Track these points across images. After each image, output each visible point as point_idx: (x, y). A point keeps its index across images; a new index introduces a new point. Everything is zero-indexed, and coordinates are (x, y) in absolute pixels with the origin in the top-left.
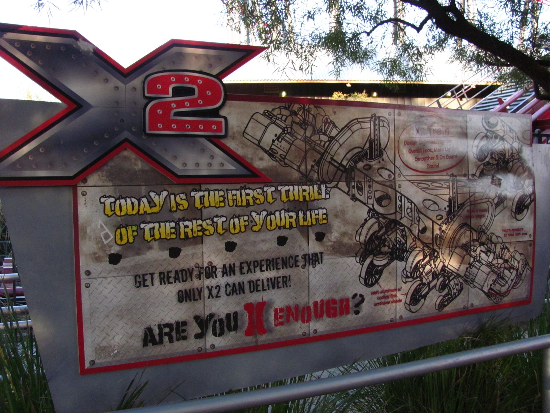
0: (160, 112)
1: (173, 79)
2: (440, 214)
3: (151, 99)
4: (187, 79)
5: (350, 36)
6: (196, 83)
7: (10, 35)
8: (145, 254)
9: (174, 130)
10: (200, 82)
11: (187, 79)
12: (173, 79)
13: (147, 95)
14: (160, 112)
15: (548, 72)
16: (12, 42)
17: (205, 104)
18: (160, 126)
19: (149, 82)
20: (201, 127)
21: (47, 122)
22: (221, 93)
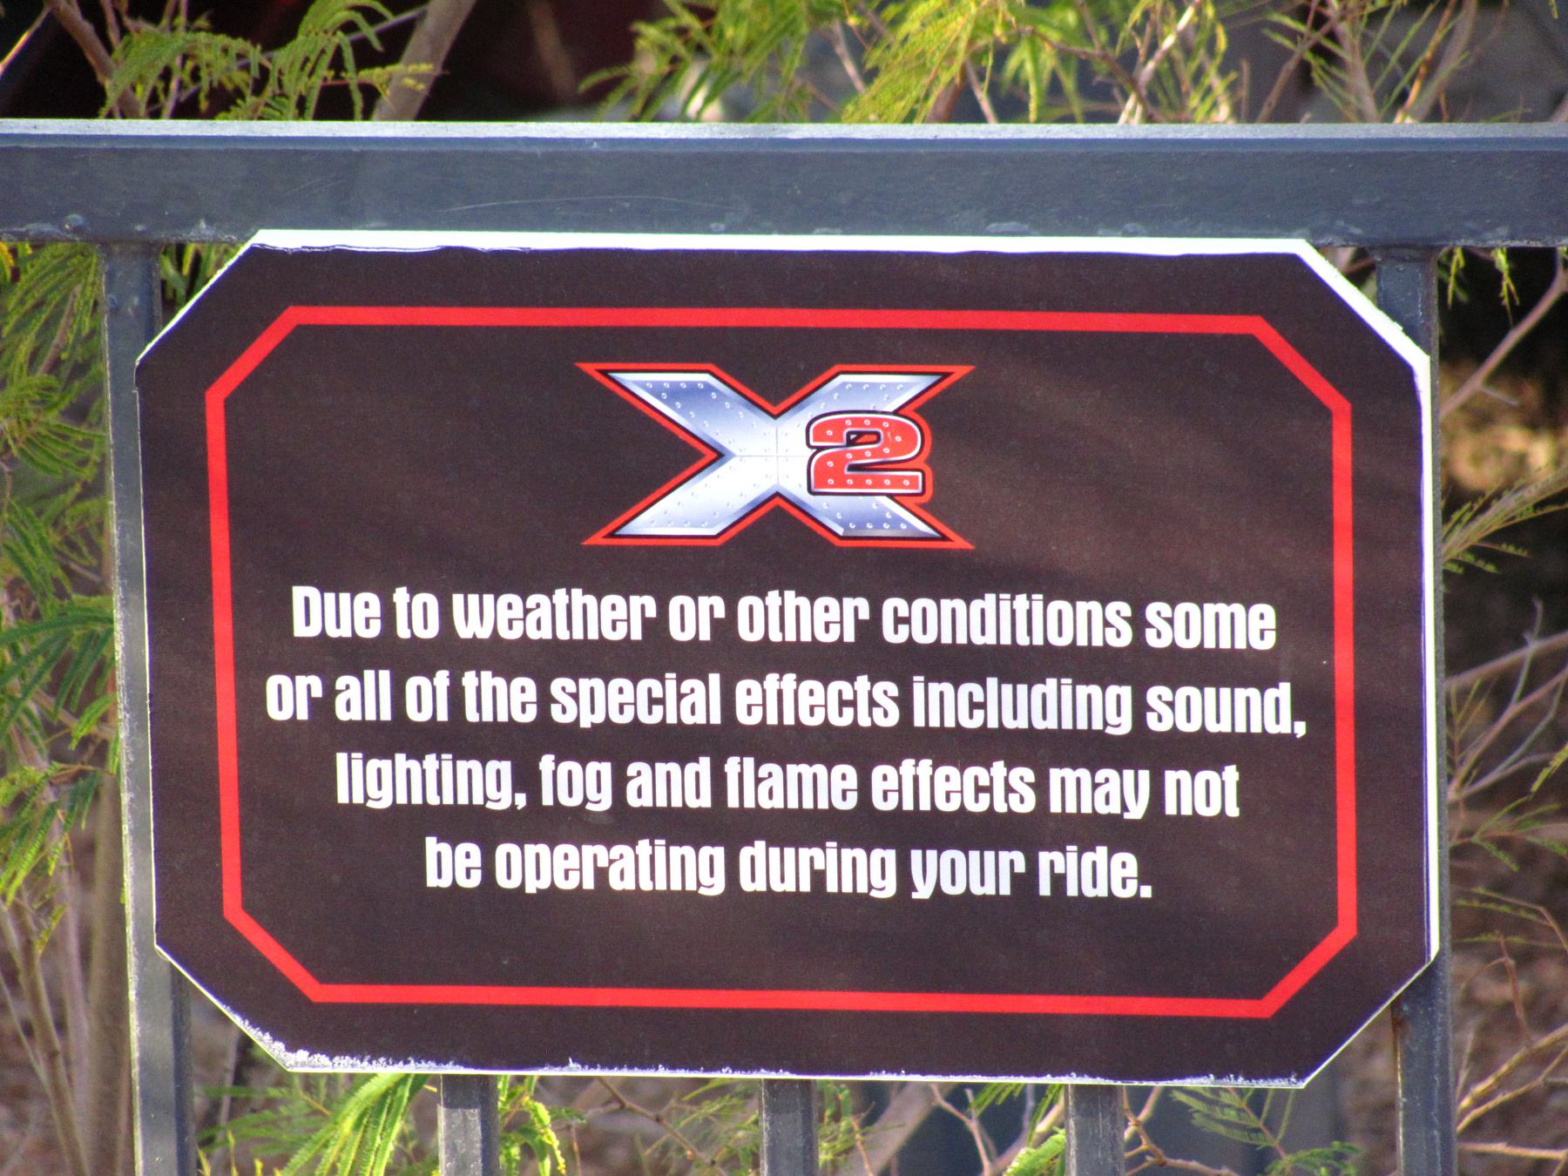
0: (830, 464)
1: (849, 422)
2: (812, 497)
3: (820, 449)
4: (867, 422)
5: (332, 73)
6: (880, 426)
7: (1454, 709)
8: (1442, 498)
9: (887, 477)
10: (886, 425)
11: (867, 422)
12: (849, 422)
13: (812, 443)
14: (830, 464)
15: (4, 5)
16: (1459, 708)
17: (893, 454)
18: (831, 481)
19: (816, 428)
20: (907, 483)
21: (809, 507)
22: (826, 422)
